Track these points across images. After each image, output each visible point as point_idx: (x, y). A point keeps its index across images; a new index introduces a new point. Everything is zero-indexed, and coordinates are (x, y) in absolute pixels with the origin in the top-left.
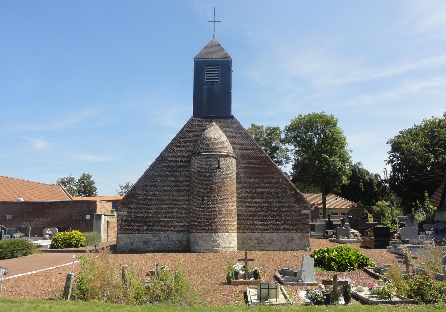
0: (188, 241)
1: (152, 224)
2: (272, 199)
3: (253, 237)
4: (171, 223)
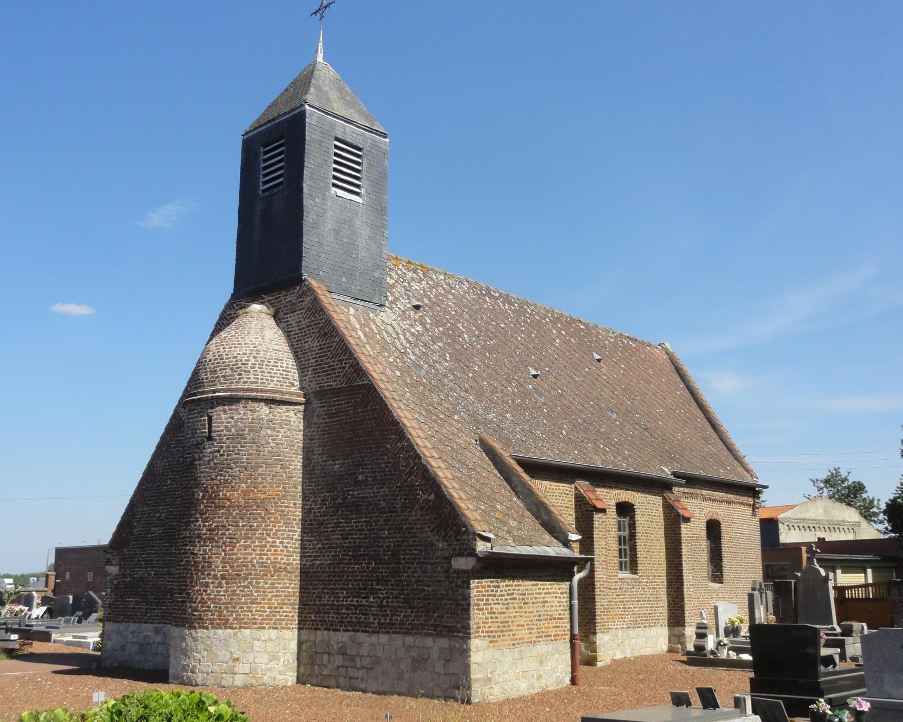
2: (380, 521)
3: (334, 644)
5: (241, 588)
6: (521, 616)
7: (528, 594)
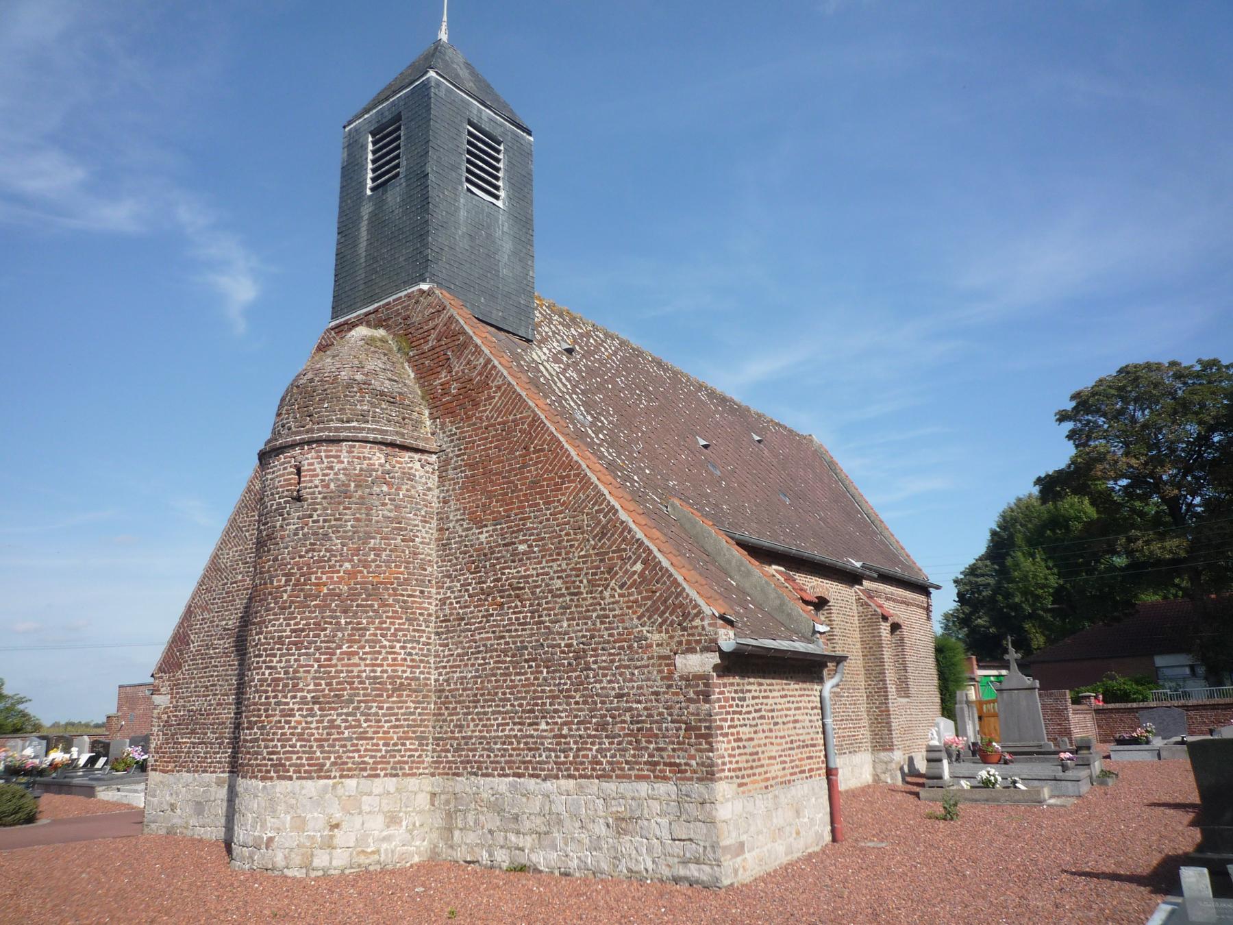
5: (344, 717)
6: (772, 744)
7: (778, 710)
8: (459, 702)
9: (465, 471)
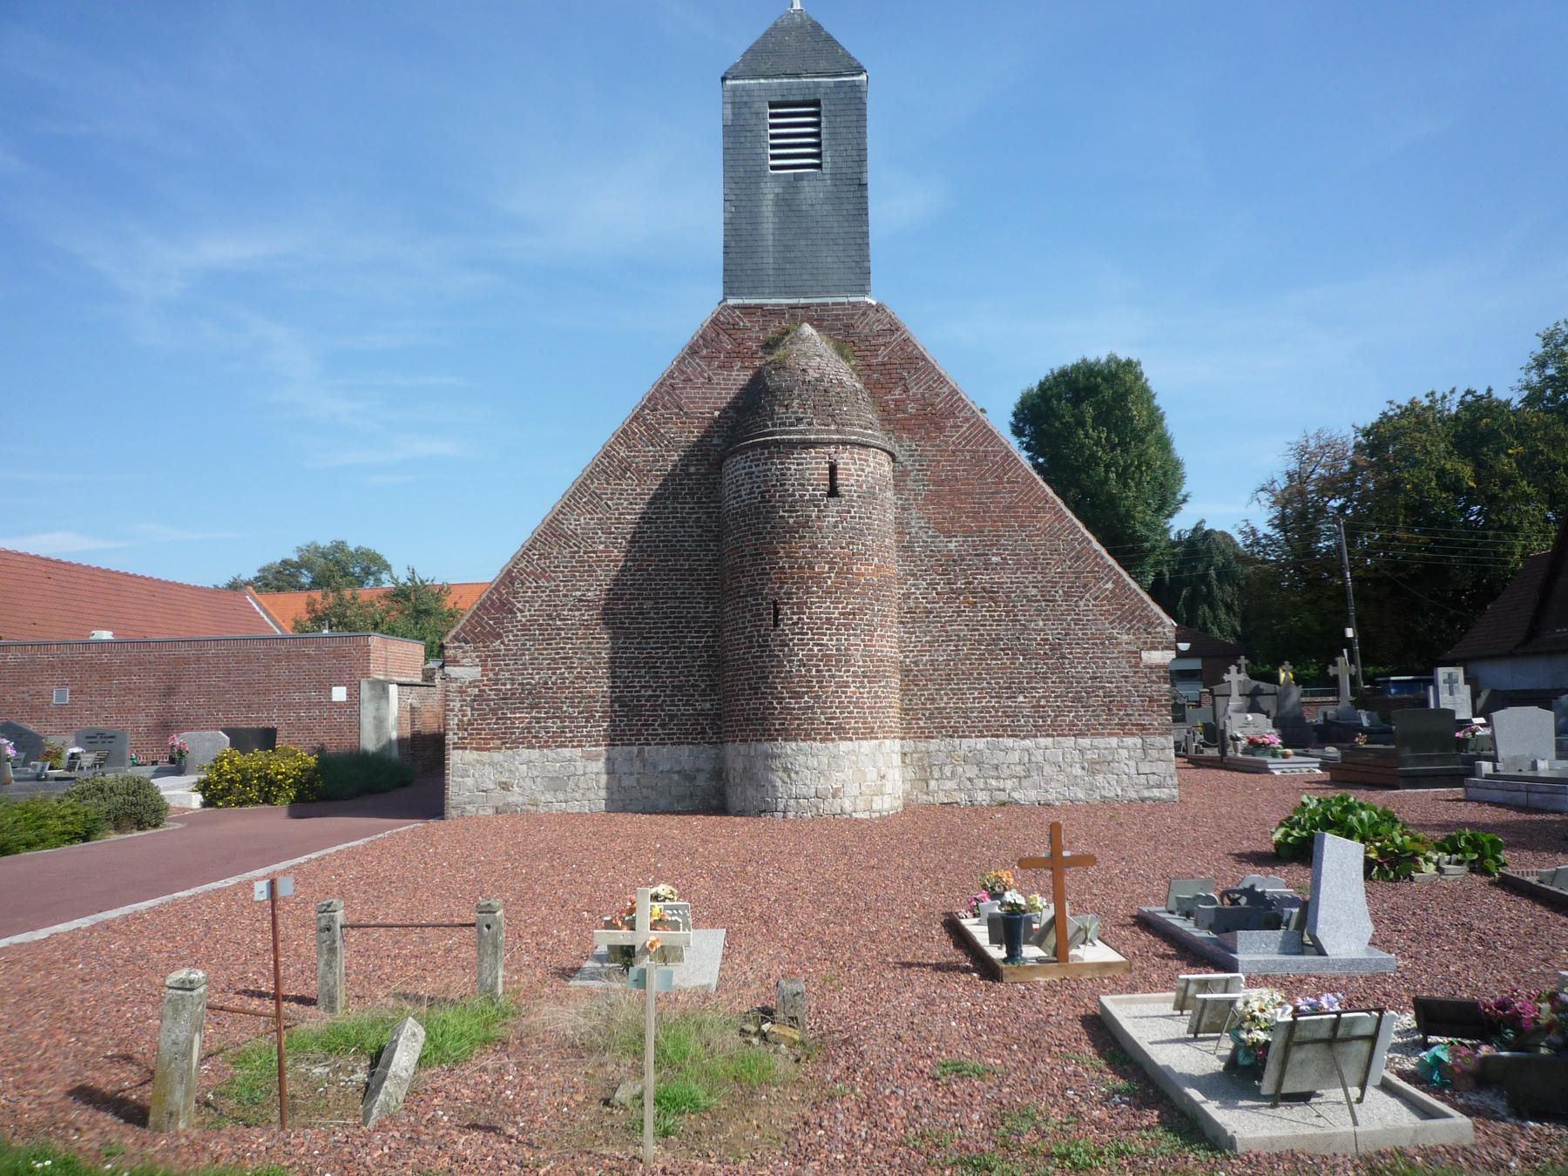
0: (719, 774)
1: (579, 713)
4: (651, 706)
8: (930, 680)
9: (928, 485)
